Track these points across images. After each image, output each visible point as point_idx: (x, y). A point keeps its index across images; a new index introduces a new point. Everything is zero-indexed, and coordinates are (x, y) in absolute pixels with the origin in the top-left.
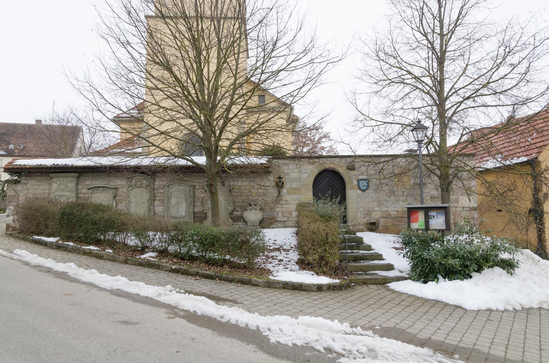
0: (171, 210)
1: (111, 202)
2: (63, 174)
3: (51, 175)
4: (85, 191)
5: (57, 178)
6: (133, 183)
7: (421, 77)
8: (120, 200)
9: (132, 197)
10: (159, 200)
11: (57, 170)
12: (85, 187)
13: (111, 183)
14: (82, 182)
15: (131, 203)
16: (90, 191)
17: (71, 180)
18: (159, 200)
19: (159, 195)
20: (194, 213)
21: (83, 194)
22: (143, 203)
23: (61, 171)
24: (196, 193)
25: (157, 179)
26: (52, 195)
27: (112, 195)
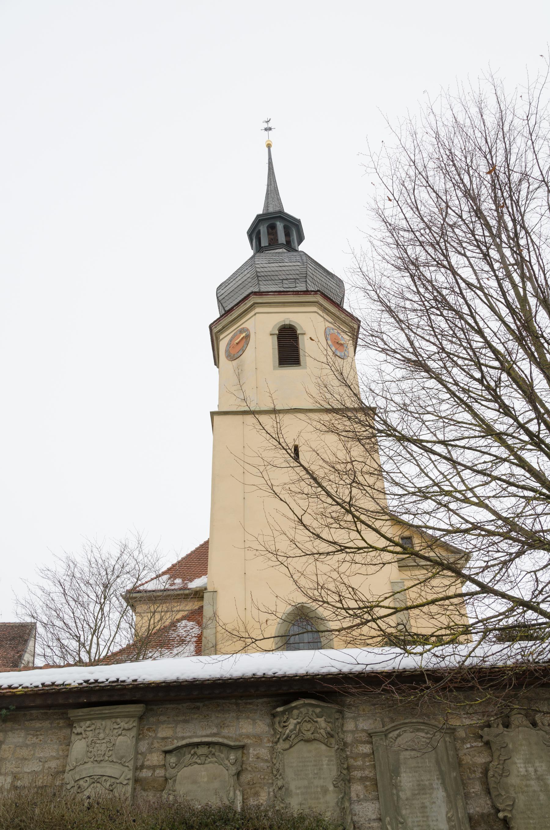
0: (404, 812)
1: (232, 794)
2: (106, 710)
3: (73, 713)
4: (155, 759)
5: (88, 723)
6: (291, 727)
7: (490, 482)
8: (252, 784)
9: (289, 773)
10: (362, 779)
11: (94, 699)
12: (156, 745)
13: (225, 732)
14: (149, 729)
15: (288, 793)
16: (172, 759)
17: (126, 726)
18: (362, 779)
19: (360, 763)
20: (470, 818)
21: (149, 767)
22: (325, 791)
23: (105, 699)
24: (461, 753)
25: (348, 715)
26: (68, 777)
27: (233, 770)
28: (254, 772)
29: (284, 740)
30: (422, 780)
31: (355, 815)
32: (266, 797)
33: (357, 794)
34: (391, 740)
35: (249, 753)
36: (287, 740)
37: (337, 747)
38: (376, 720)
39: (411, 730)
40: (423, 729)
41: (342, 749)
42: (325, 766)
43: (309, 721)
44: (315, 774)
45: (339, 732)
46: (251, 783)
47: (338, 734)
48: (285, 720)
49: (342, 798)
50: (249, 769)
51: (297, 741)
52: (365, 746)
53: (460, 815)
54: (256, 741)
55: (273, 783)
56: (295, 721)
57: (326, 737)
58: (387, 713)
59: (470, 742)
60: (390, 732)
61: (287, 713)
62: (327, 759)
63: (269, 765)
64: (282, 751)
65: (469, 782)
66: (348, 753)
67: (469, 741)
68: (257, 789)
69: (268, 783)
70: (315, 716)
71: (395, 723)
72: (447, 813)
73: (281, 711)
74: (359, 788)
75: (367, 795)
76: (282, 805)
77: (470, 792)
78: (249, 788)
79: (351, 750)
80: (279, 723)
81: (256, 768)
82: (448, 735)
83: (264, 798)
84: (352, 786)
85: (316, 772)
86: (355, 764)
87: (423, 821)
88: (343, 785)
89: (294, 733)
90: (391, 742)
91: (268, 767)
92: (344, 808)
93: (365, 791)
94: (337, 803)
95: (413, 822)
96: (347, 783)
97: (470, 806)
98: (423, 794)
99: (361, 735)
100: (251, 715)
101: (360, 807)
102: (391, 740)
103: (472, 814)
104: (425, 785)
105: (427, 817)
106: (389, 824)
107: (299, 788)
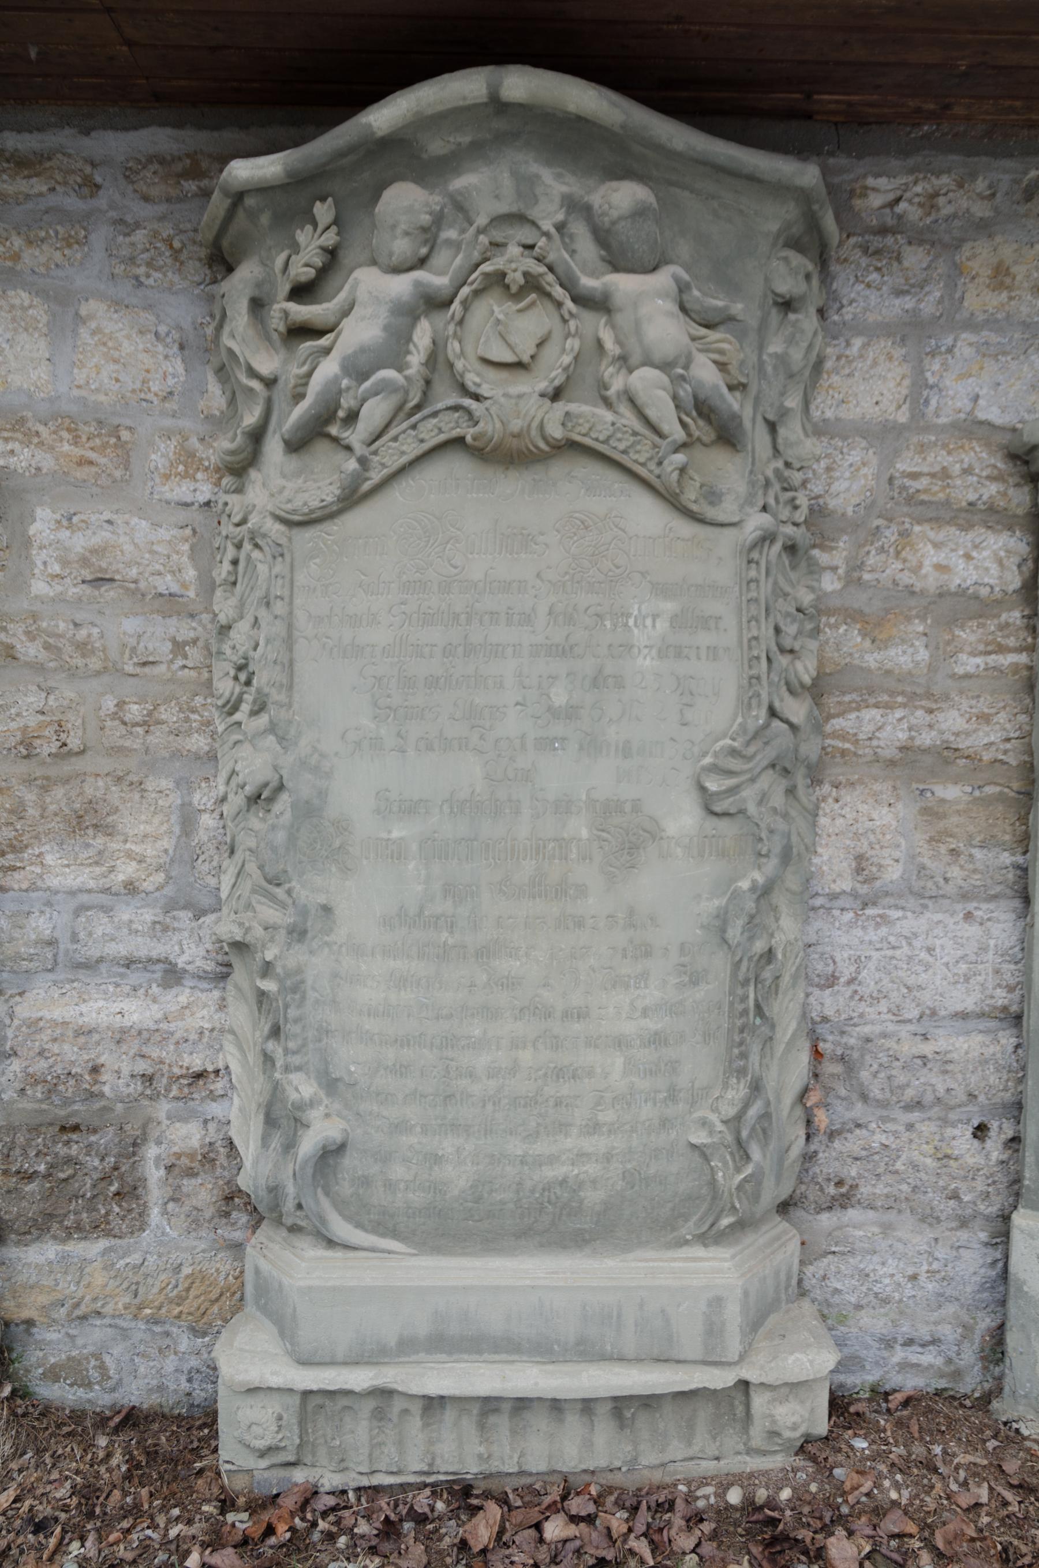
28: (72, 673)
29: (296, 445)
31: (831, 981)
32: (166, 843)
33: (860, 858)
35: (28, 543)
36: (322, 447)
37: (756, 522)
41: (791, 548)
42: (646, 662)
43: (532, 285)
44: (553, 712)
45: (784, 413)
46: (47, 748)
47: (772, 427)
48: (302, 271)
49: (764, 892)
50: (31, 650)
51: (413, 450)
52: (966, 539)
54: (84, 462)
55: (212, 757)
56: (401, 285)
57: (679, 434)
61: (323, 211)
62: (669, 607)
63: (185, 630)
64: (275, 529)
66: (829, 583)
68: (94, 788)
69: (177, 754)
70: (587, 247)
73: (264, 190)
74: (883, 816)
76: (269, 913)
78: (29, 781)
79: (856, 566)
80: (257, 305)
81: (83, 648)
83: (149, 850)
84: (828, 806)
85: (559, 697)
86: (871, 660)
88: (778, 800)
89: (383, 388)
91: (179, 647)
92: (769, 955)
93: (920, 838)
94: (721, 923)
96: (801, 780)
100: (32, 258)
101: (872, 935)
107: (410, 809)
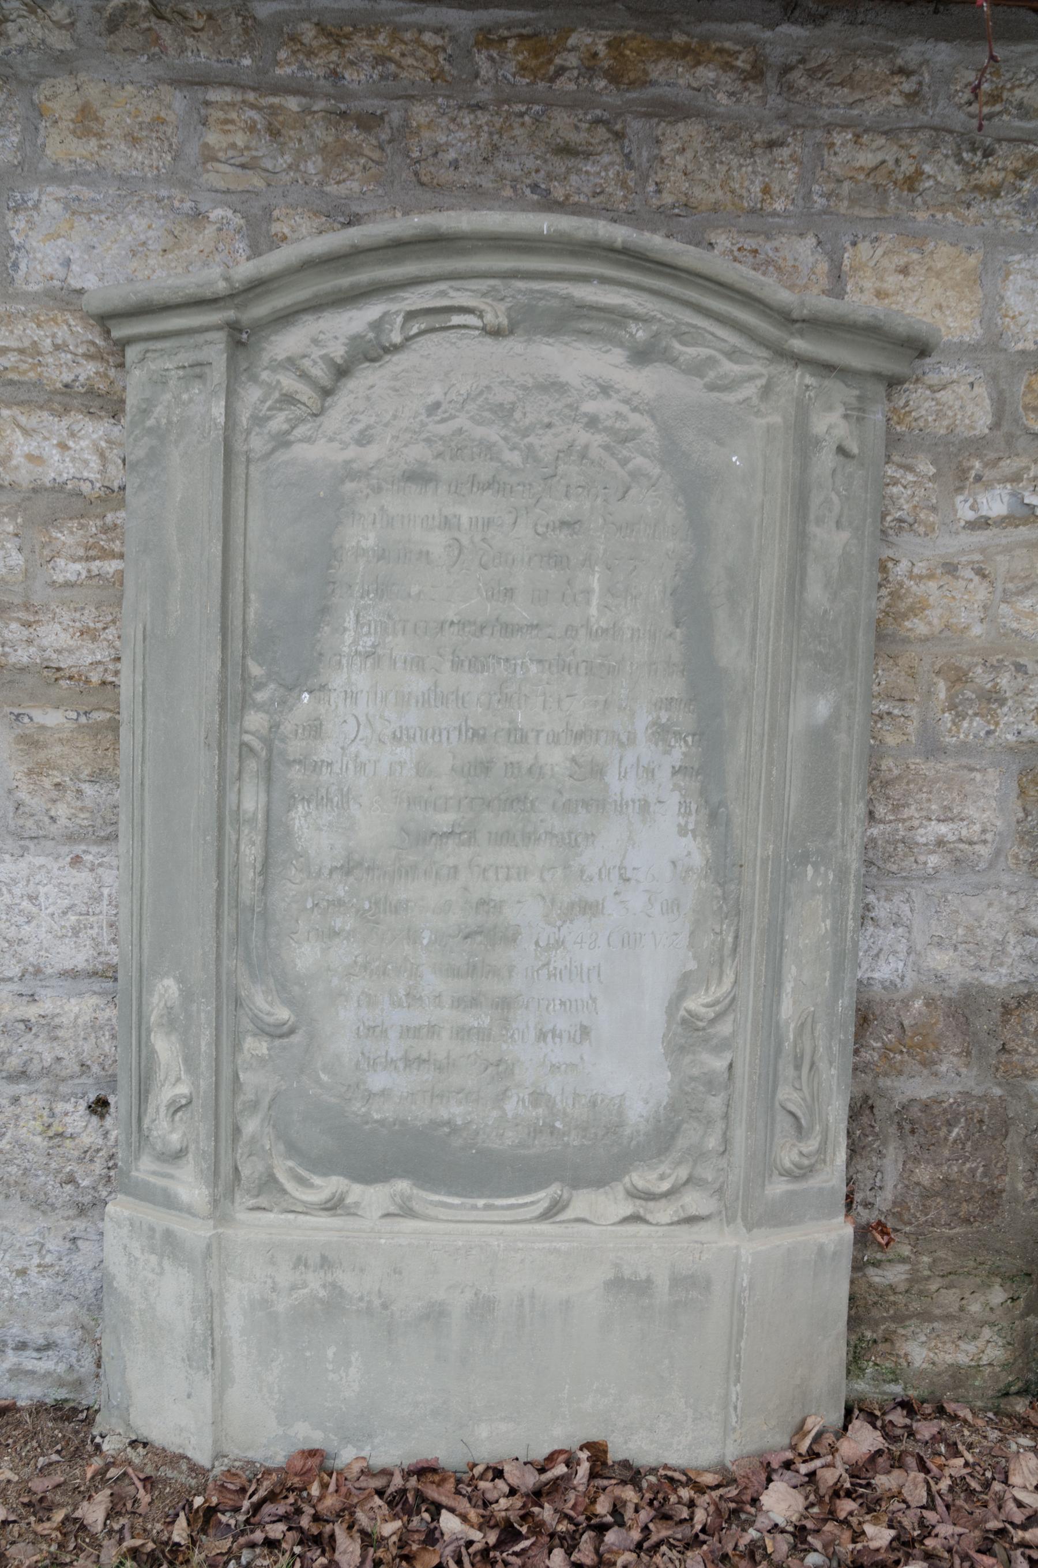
30: (518, 736)
34: (289, 382)
38: (198, 217)
39: (496, 314)
40: (621, 316)
53: (787, 1009)
58: (313, 166)
59: (1015, 478)
60: (286, 318)
65: (928, 768)
67: (1009, 466)
71: (355, 235)
72: (685, 985)
75: (35, 803)
77: (909, 845)
82: (841, 392)
87: (462, 1033)
90: (289, 399)
95: (375, 1031)
97: (888, 937)
98: (504, 838)
99: (34, 332)
102: (289, 382)
103: (890, 986)
104: (536, 771)
105: (505, 1004)
106: (171, 1022)
